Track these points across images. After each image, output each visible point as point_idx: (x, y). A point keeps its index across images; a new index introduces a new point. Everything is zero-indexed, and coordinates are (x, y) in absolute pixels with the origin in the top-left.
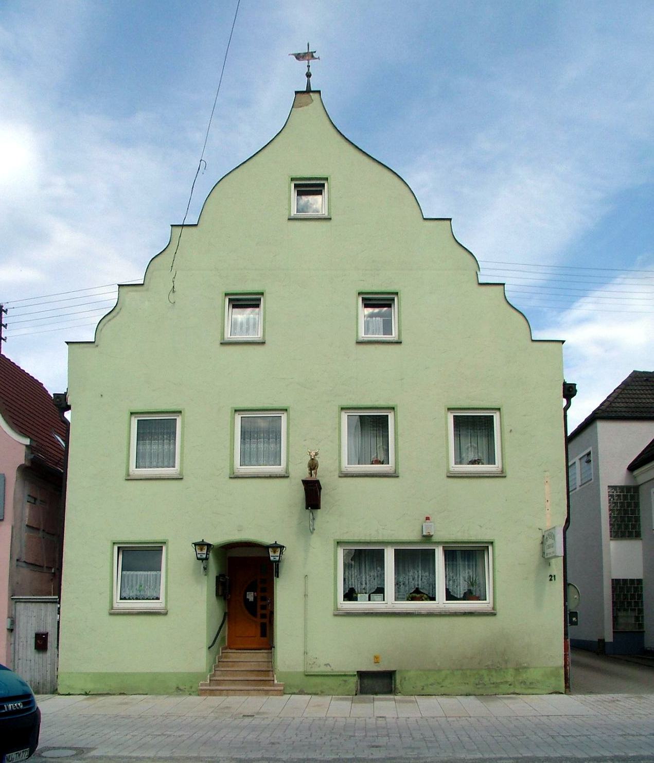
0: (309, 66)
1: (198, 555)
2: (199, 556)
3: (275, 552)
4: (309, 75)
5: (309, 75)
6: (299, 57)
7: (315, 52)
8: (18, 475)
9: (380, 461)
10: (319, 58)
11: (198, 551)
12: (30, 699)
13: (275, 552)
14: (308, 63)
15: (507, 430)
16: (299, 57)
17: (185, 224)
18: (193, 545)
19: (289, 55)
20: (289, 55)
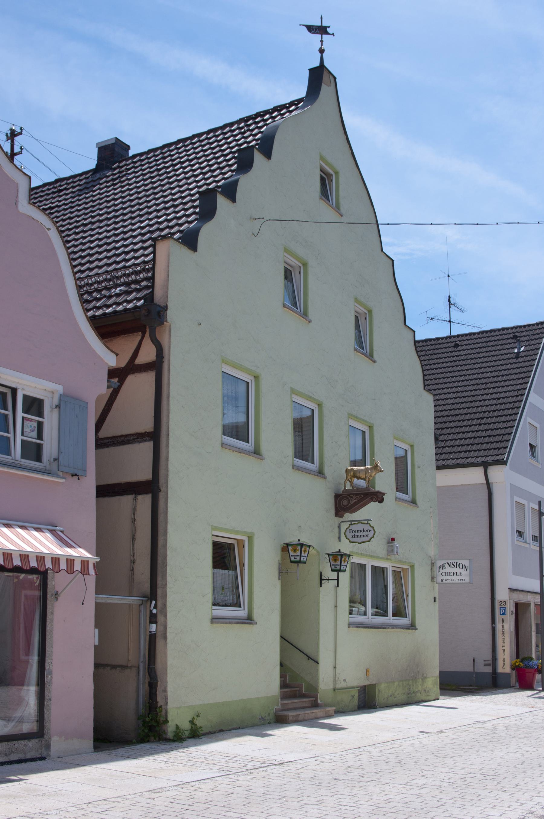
0: (322, 41)
1: (332, 566)
2: (333, 567)
3: (295, 551)
4: (322, 51)
5: (322, 51)
6: (311, 29)
7: (329, 27)
8: (361, 487)
9: (119, 386)
10: (333, 34)
11: (332, 563)
12: (283, 690)
13: (295, 551)
14: (322, 38)
15: (242, 403)
16: (311, 29)
17: (379, 225)
18: (327, 556)
19: (300, 25)
20: (300, 25)
